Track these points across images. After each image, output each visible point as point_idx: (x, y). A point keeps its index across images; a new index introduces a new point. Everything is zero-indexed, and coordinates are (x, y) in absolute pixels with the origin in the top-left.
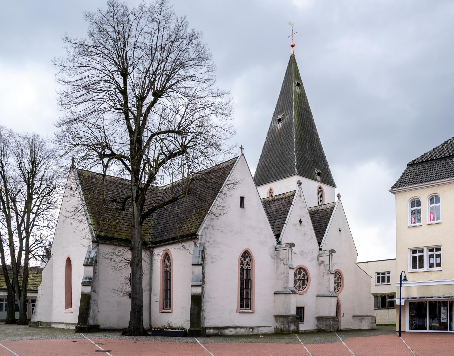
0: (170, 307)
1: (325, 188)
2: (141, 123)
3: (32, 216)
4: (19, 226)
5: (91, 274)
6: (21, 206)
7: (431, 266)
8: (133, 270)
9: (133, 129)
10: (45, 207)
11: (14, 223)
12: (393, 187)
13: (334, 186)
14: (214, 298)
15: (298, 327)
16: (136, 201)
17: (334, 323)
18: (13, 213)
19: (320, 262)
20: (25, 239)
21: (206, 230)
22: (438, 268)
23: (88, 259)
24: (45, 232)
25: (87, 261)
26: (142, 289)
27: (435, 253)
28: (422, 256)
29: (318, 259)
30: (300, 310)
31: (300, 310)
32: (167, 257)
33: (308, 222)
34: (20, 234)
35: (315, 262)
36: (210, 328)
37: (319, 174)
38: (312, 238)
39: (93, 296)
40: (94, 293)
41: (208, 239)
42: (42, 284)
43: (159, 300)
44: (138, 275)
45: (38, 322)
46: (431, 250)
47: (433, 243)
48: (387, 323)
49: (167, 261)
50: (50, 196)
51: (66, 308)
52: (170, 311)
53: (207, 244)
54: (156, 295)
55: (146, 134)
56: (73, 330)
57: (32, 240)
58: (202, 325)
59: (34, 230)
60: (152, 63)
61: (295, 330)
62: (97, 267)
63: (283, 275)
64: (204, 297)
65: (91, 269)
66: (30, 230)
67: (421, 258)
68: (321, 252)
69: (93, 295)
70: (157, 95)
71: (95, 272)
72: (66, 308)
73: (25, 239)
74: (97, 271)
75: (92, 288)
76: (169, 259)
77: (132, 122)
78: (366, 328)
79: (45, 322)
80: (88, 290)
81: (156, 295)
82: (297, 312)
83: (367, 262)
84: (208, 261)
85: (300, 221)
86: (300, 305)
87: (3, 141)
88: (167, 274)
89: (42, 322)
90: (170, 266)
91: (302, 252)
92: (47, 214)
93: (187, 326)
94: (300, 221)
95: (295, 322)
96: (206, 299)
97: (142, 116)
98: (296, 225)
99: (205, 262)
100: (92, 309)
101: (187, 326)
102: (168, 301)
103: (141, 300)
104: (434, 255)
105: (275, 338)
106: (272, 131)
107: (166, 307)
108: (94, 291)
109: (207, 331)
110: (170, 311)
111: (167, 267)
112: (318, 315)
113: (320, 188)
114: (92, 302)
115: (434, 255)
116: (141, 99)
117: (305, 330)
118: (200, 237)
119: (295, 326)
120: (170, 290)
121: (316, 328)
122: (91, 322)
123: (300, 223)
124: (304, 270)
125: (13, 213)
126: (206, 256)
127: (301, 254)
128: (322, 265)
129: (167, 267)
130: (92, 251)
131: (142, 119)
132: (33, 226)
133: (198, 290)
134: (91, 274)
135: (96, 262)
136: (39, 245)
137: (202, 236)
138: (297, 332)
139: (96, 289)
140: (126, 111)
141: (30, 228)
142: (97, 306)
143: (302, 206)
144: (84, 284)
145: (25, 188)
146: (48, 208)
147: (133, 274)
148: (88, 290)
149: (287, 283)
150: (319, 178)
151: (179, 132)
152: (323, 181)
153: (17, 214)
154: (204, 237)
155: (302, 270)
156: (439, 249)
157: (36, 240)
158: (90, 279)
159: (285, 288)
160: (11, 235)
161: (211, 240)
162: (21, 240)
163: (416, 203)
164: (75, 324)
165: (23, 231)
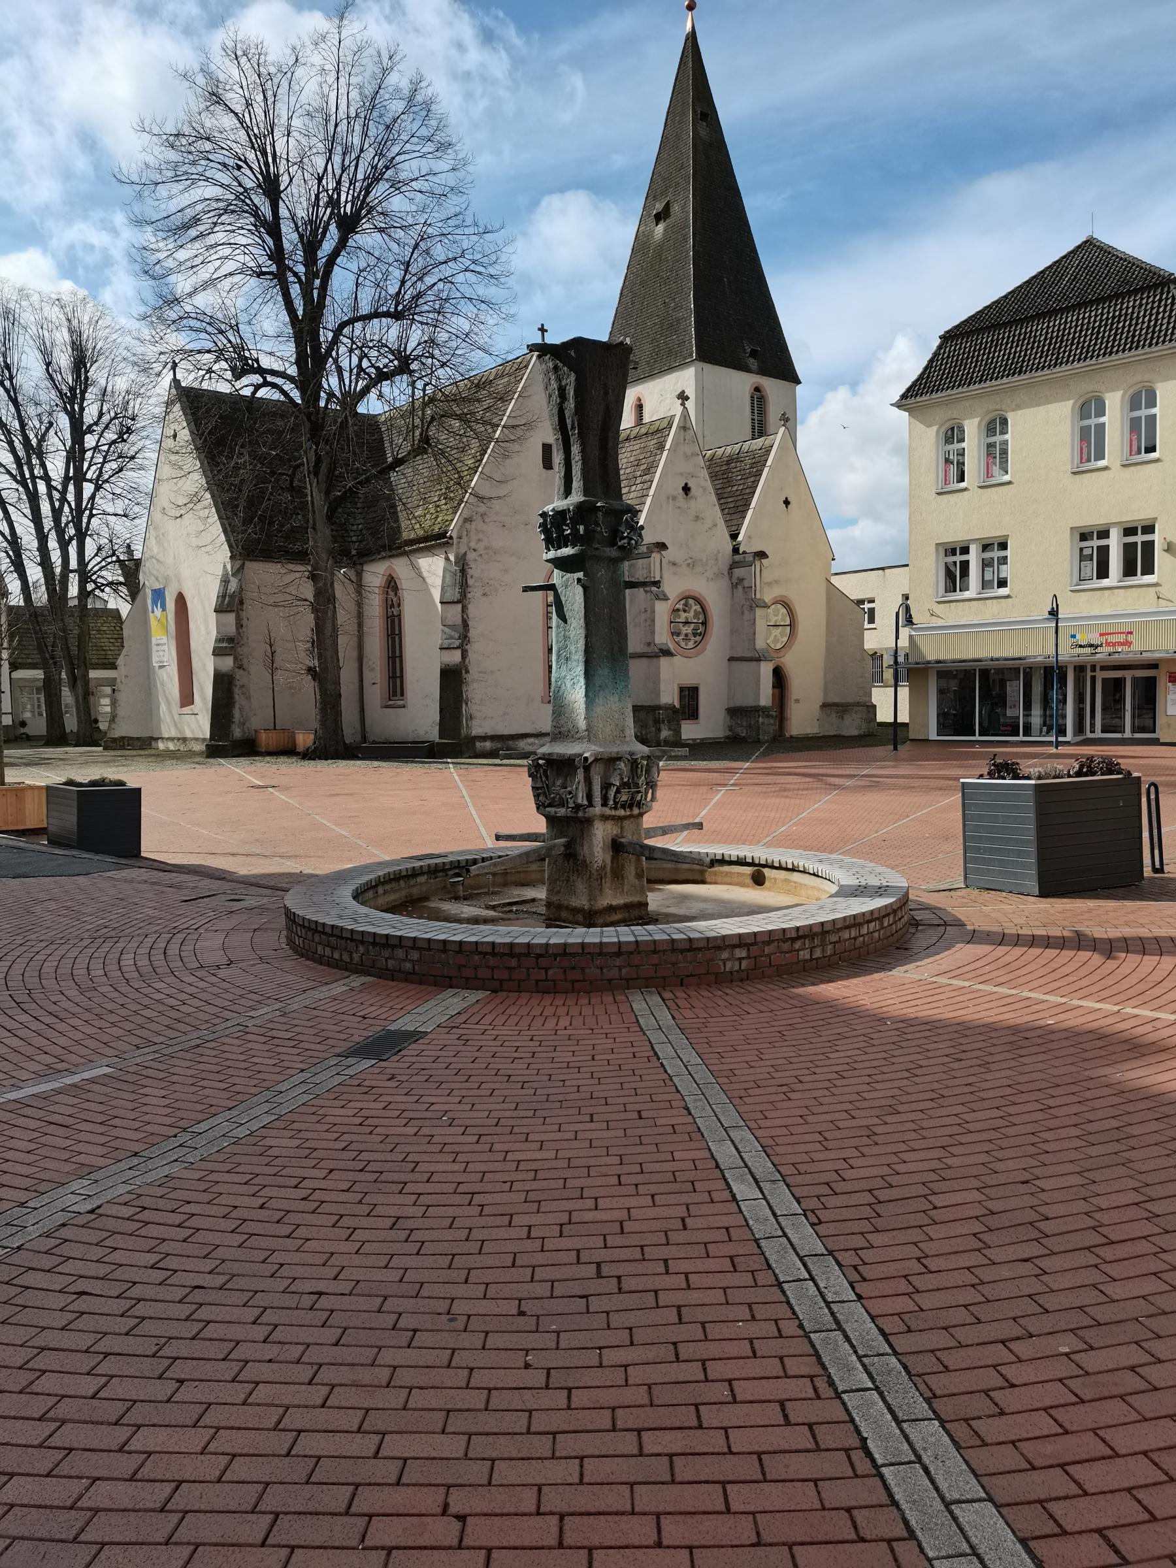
0: (402, 695)
1: (770, 385)
2: (315, 293)
3: (88, 489)
4: (57, 514)
5: (232, 630)
6: (56, 466)
7: (985, 584)
8: (317, 618)
9: (300, 313)
10: (114, 465)
11: (45, 508)
12: (904, 396)
13: (798, 382)
14: (492, 672)
15: (677, 731)
16: (316, 474)
17: (766, 721)
18: (42, 487)
19: (735, 581)
20: (74, 542)
21: (467, 525)
22: (1003, 591)
23: (224, 596)
24: (120, 526)
25: (223, 602)
26: (338, 660)
27: (996, 554)
28: (968, 562)
29: (731, 577)
30: (690, 694)
31: (690, 694)
32: (391, 585)
33: (704, 489)
34: (60, 532)
35: (724, 583)
36: (484, 738)
37: (753, 354)
38: (715, 525)
39: (238, 677)
40: (241, 671)
41: (473, 545)
42: (124, 652)
43: (378, 681)
44: (328, 630)
45: (123, 738)
46: (986, 547)
47: (992, 532)
48: (892, 720)
49: (391, 594)
50: (125, 441)
51: (183, 705)
52: (401, 703)
53: (471, 556)
54: (373, 670)
55: (330, 320)
56: (200, 754)
57: (90, 546)
58: (464, 732)
59: (95, 522)
60: (330, 158)
61: (671, 739)
62: (243, 614)
63: (644, 616)
64: (467, 672)
65: (231, 618)
66: (84, 525)
67: (965, 565)
68: (737, 558)
69: (239, 674)
70: (349, 225)
71: (239, 625)
72: (183, 705)
73: (74, 542)
74: (244, 622)
75: (236, 659)
76: (396, 589)
77: (295, 290)
78: (855, 732)
79: (138, 739)
80: (228, 663)
81: (373, 670)
82: (681, 698)
83: (883, 569)
84: (474, 593)
85: (686, 489)
86: (689, 681)
87: (7, 314)
88: (393, 622)
89: (131, 738)
90: (399, 605)
91: (690, 561)
92: (119, 484)
93: (434, 735)
94: (686, 489)
95: (669, 722)
96: (473, 675)
97: (316, 276)
98: (674, 498)
99: (469, 595)
100: (237, 706)
101: (434, 735)
102: (398, 680)
103: (337, 683)
104: (992, 559)
105: (159, 687)
106: (641, 245)
107: (395, 695)
108: (240, 667)
109: (478, 744)
110: (401, 703)
111: (392, 606)
112: (732, 705)
113: (757, 389)
114: (236, 690)
115: (992, 559)
116: (311, 246)
117: (702, 739)
118: (455, 541)
119: (670, 729)
120: (401, 657)
121: (728, 733)
122: (237, 733)
123: (687, 494)
124: (698, 600)
125: (42, 487)
126: (470, 582)
127: (688, 565)
128: (740, 587)
129: (392, 606)
130: (232, 579)
131: (317, 282)
132: (91, 516)
133: (455, 657)
134: (232, 630)
135: (241, 603)
136: (109, 560)
137: (460, 537)
138: (678, 743)
139: (245, 661)
140: (280, 277)
141: (85, 520)
142: (249, 698)
143: (689, 452)
144: (217, 652)
145: (63, 421)
146: (121, 470)
147: (319, 629)
148: (228, 663)
149: (653, 633)
150: (753, 363)
151: (397, 316)
152: (764, 372)
153: (50, 488)
154: (464, 540)
155: (691, 601)
156: (1003, 546)
157: (100, 549)
158: (231, 640)
159: (649, 644)
160: (42, 538)
161: (480, 546)
162: (64, 545)
163: (953, 434)
164: (204, 740)
165: (66, 525)
